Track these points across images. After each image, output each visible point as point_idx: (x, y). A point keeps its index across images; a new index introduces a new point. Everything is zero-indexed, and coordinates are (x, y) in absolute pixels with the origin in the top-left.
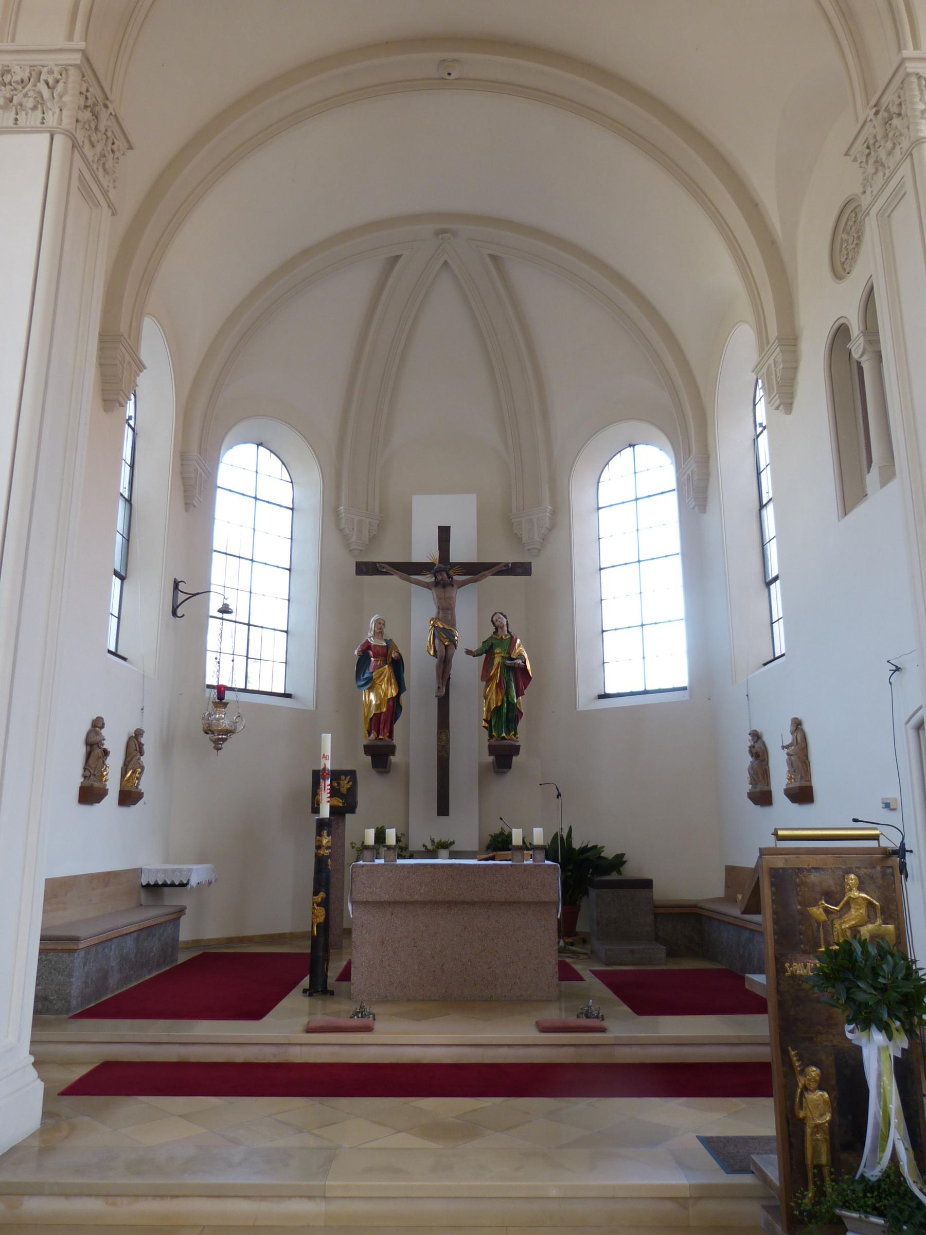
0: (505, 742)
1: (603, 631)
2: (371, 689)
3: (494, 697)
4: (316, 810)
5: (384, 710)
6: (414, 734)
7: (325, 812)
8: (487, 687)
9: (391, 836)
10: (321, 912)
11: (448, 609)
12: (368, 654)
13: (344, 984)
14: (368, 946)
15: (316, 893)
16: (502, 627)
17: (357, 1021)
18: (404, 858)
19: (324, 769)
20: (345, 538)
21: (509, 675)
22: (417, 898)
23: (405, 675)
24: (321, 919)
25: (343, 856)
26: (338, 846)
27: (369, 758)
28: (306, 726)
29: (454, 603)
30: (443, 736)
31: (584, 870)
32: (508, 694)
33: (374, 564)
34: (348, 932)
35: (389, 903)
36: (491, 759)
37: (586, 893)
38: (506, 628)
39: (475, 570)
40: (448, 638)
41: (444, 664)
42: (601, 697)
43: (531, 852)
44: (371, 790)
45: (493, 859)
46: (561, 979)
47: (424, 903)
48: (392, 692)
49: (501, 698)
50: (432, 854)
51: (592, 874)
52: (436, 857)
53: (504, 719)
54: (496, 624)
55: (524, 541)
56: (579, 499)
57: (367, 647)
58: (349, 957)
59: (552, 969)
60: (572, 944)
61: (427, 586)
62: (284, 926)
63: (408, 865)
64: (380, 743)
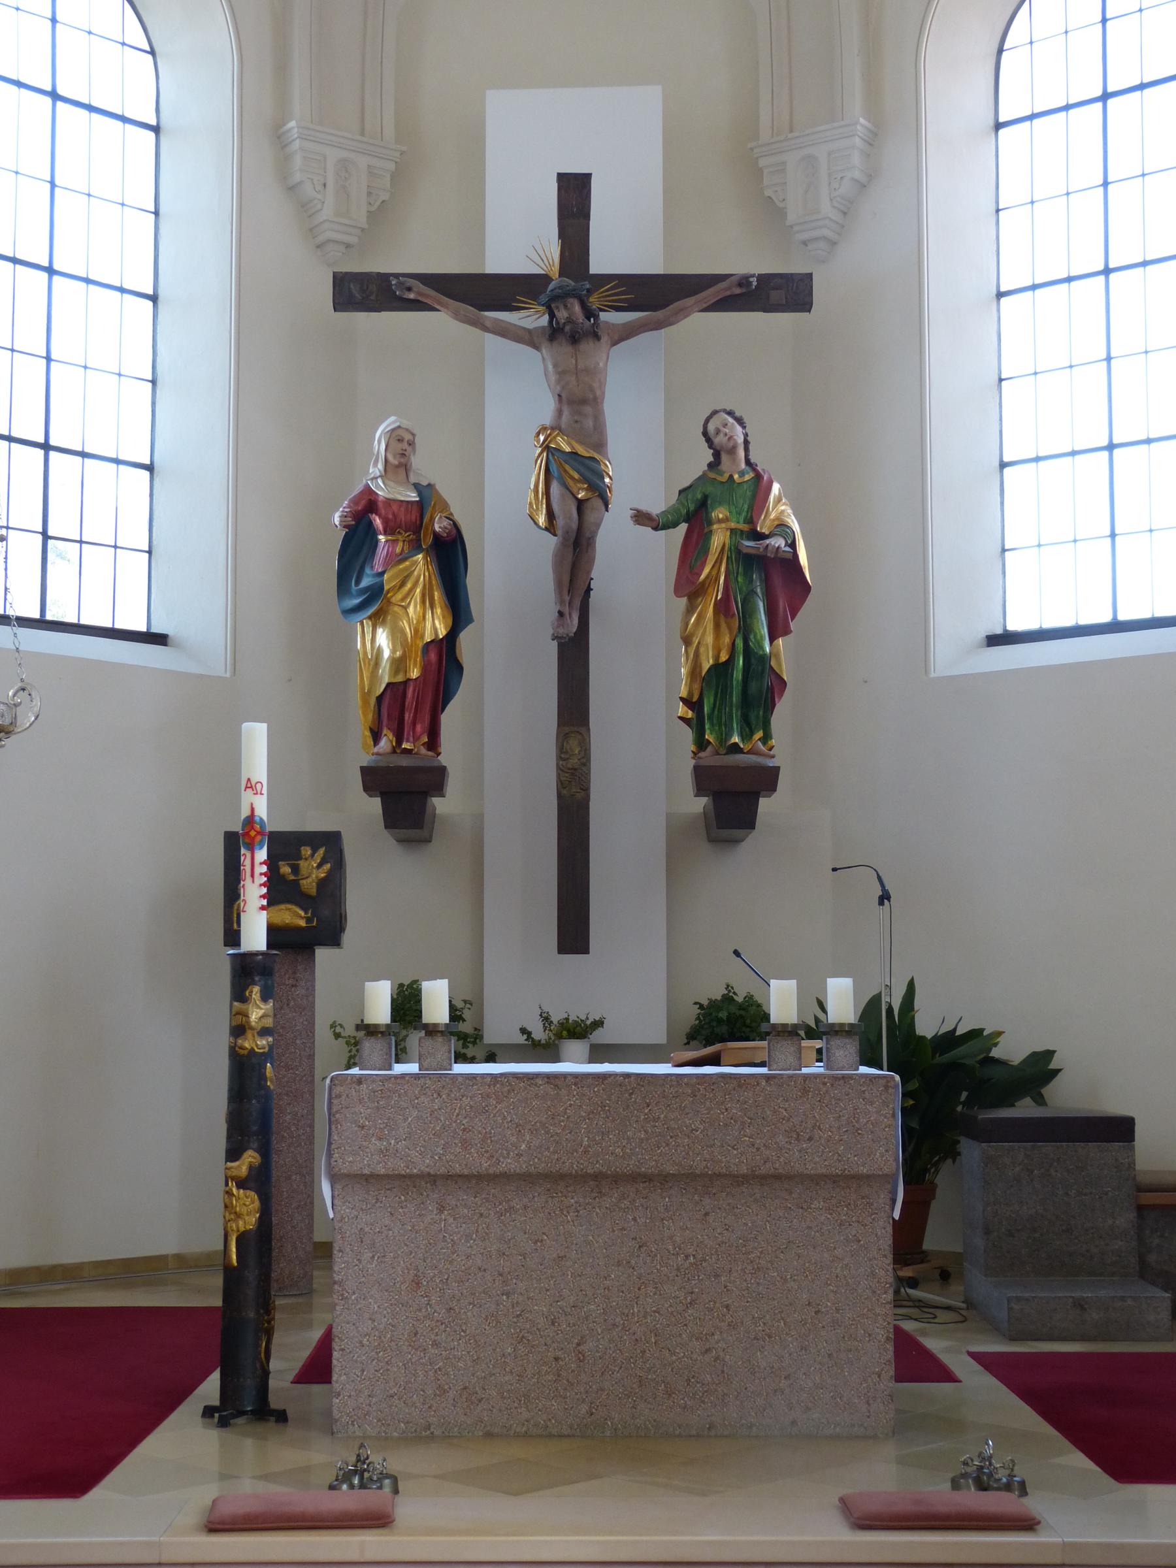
0: (739, 758)
1: (1003, 465)
2: (378, 618)
3: (709, 639)
4: (232, 936)
5: (415, 673)
6: (495, 739)
7: (255, 935)
8: (690, 611)
9: (436, 1001)
10: (248, 1203)
11: (584, 402)
12: (370, 524)
13: (316, 1388)
14: (378, 1286)
15: (233, 1154)
16: (732, 451)
17: (348, 1499)
18: (472, 1060)
19: (250, 820)
20: (305, 209)
21: (749, 579)
22: (509, 1164)
23: (471, 581)
24: (250, 1222)
25: (311, 1057)
26: (294, 1028)
27: (376, 802)
28: (207, 715)
29: (602, 385)
30: (573, 744)
31: (952, 1091)
32: (746, 630)
33: (384, 278)
34: (325, 1250)
35: (432, 1179)
36: (701, 804)
37: (954, 1154)
38: (741, 453)
39: (656, 296)
40: (585, 479)
41: (576, 551)
42: (994, 640)
43: (818, 1044)
44: (380, 883)
45: (715, 1060)
46: (899, 1378)
47: (528, 1179)
48: (437, 625)
49: (727, 640)
50: (547, 1051)
51: (968, 1103)
52: (556, 1059)
53: (735, 698)
55: (791, 218)
56: (948, 96)
57: (366, 507)
58: (327, 1317)
59: (879, 1354)
60: (913, 1283)
62: (162, 1238)
63: (483, 1076)
64: (404, 761)
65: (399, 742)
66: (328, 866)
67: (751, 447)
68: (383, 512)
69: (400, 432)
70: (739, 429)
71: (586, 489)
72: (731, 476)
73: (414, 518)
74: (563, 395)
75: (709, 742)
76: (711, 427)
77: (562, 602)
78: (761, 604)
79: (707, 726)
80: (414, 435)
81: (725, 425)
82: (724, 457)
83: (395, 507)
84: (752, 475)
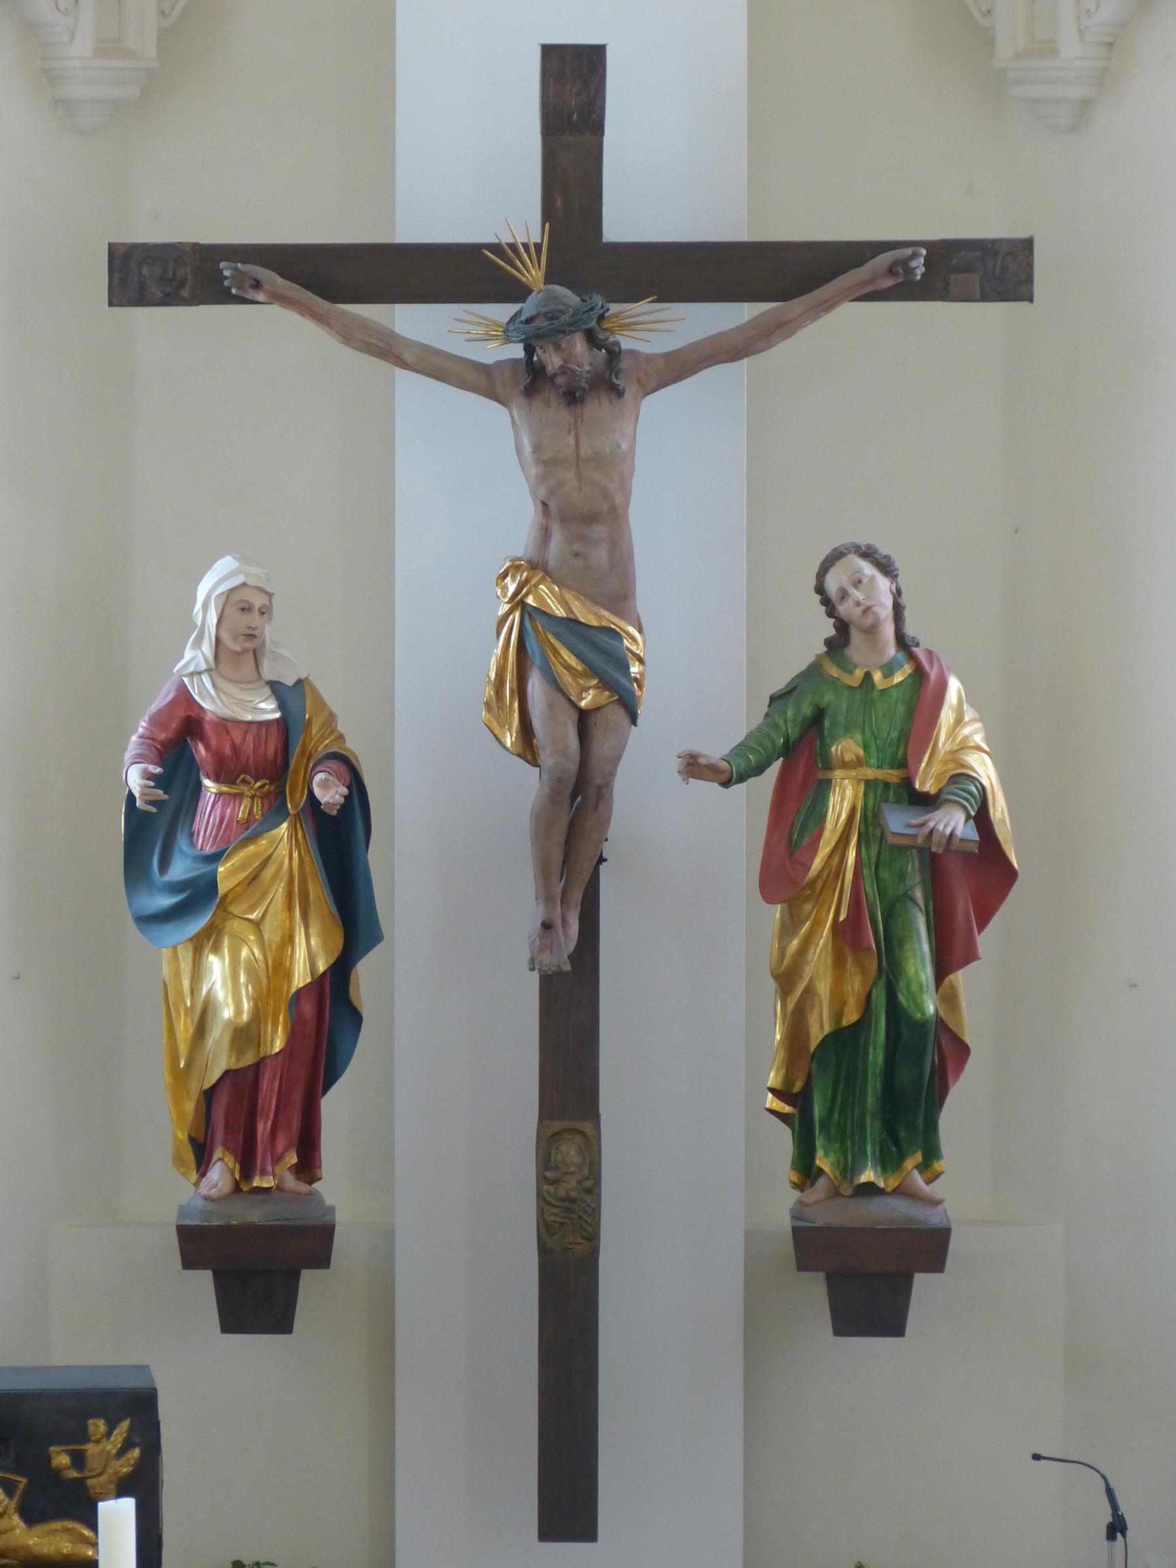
6: (423, 1143)
11: (591, 518)
16: (872, 631)
23: (375, 857)
30: (570, 1152)
32: (890, 971)
38: (889, 630)
40: (592, 671)
53: (871, 1085)
54: (843, 609)
55: (1004, 51)
57: (181, 741)
61: (482, 380)
64: (255, 1214)
65: (247, 1172)
66: (136, 1452)
67: (907, 614)
68: (213, 742)
69: (245, 594)
70: (884, 584)
71: (596, 687)
72: (868, 676)
73: (271, 752)
74: (552, 505)
75: (821, 1172)
76: (832, 583)
77: (547, 898)
78: (921, 923)
79: (819, 1143)
80: (270, 595)
81: (857, 583)
82: (855, 636)
83: (237, 735)
84: (908, 669)
